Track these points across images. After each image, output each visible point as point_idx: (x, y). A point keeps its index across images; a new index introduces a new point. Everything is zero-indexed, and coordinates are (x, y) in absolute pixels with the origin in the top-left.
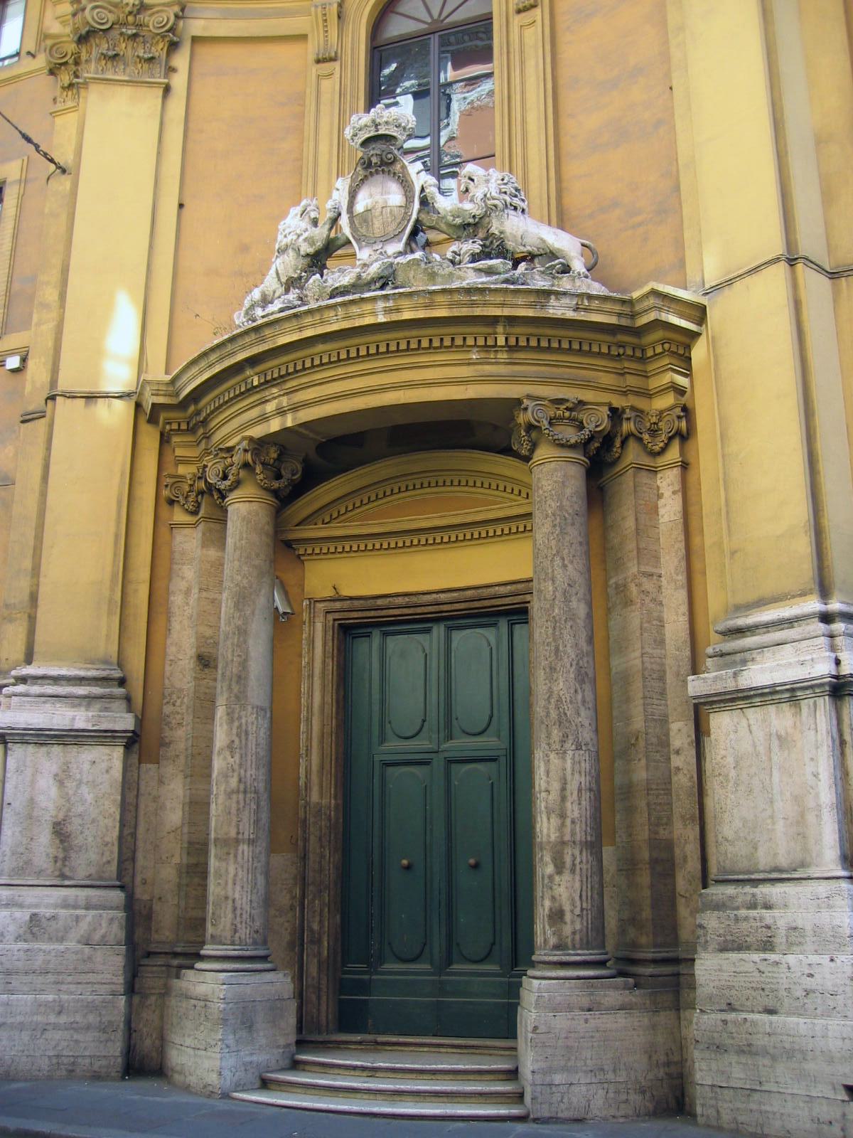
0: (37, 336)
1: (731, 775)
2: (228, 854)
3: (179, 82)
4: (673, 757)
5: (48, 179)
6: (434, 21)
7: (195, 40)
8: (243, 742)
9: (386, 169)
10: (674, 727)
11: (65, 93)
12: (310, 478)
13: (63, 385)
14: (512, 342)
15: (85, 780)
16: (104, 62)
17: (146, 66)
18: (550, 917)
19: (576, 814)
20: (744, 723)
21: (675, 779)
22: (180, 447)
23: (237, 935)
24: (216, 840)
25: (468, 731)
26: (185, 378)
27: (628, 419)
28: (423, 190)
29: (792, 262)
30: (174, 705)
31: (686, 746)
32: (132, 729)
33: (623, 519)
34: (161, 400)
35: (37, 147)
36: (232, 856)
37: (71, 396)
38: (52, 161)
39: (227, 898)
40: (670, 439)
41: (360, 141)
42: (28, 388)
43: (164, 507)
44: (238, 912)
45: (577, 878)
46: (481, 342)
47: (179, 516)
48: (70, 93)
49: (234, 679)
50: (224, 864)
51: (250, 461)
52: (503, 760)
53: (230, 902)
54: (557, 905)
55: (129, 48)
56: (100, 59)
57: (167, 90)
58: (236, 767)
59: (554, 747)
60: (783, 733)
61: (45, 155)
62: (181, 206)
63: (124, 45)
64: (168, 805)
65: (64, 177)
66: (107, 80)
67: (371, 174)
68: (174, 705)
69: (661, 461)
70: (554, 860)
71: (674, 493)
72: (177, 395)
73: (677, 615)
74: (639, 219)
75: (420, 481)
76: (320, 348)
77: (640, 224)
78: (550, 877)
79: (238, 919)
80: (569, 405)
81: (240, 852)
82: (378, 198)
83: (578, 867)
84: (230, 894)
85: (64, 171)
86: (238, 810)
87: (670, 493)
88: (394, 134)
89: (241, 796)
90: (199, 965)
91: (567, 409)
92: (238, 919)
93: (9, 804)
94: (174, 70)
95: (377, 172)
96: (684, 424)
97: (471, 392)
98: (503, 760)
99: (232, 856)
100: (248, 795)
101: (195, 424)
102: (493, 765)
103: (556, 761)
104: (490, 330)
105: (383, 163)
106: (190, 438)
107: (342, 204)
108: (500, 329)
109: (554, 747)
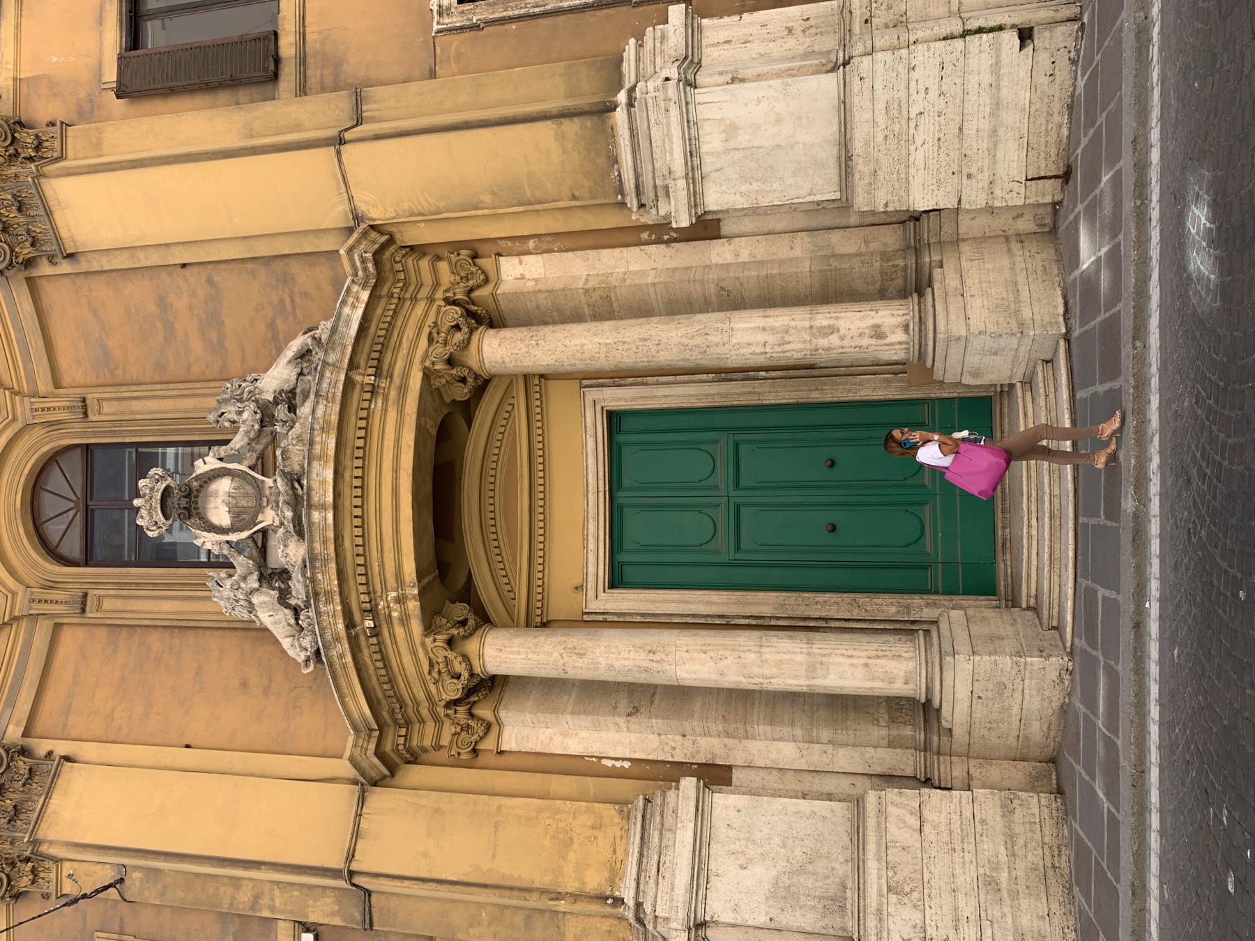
0: (280, 905)
1: (757, 188)
2: (822, 663)
3: (61, 748)
4: (740, 260)
5: (125, 900)
6: (77, 503)
7: (26, 734)
8: (711, 647)
9: (195, 493)
10: (715, 259)
11: (40, 880)
12: (468, 594)
13: (336, 862)
14: (372, 371)
15: (747, 835)
16: (19, 822)
17: (36, 779)
18: (877, 326)
19: (787, 318)
20: (714, 175)
21: (759, 258)
22: (422, 740)
23: (904, 654)
24: (808, 678)
25: (710, 470)
26: (356, 715)
27: (454, 294)
28: (221, 459)
29: (341, 141)
30: (674, 749)
31: (731, 247)
32: (695, 779)
33: (538, 308)
34: (372, 746)
35: (85, 896)
36: (824, 659)
37: (351, 856)
38: (106, 888)
39: (866, 665)
40: (475, 265)
41: (163, 519)
42: (337, 921)
43: (482, 759)
44: (880, 653)
45: (842, 315)
46: (368, 396)
47: (488, 744)
48: (42, 875)
49: (651, 656)
50: (832, 667)
51: (445, 637)
52: (737, 437)
53: (870, 661)
54: (867, 331)
55: (12, 796)
56: (14, 826)
57: (67, 759)
58: (736, 654)
59: (726, 339)
60: (723, 136)
61: (97, 891)
62: (188, 746)
63: (8, 801)
64: (774, 756)
65: (127, 882)
66: (38, 818)
67: (196, 508)
68: (674, 749)
69: (492, 274)
70: (826, 335)
71: (521, 262)
72: (372, 730)
73: (621, 258)
74: (288, 302)
75: (492, 549)
76: (347, 543)
77: (293, 301)
78: (842, 338)
79: (887, 653)
80: (434, 331)
81: (818, 651)
82: (219, 500)
83: (833, 315)
84: (862, 661)
85: (121, 880)
86: (778, 652)
87: (521, 267)
88: (164, 486)
89: (764, 650)
90: (936, 703)
91: (438, 333)
92: (887, 653)
93: (771, 920)
94: (50, 753)
95: (196, 503)
96: (463, 252)
97: (409, 438)
98: (737, 437)
99: (824, 659)
100: (764, 644)
101: (408, 751)
102: (743, 449)
103: (739, 336)
104: (358, 387)
105: (188, 496)
106: (416, 726)
107: (214, 539)
108: (358, 378)
109: (726, 339)
